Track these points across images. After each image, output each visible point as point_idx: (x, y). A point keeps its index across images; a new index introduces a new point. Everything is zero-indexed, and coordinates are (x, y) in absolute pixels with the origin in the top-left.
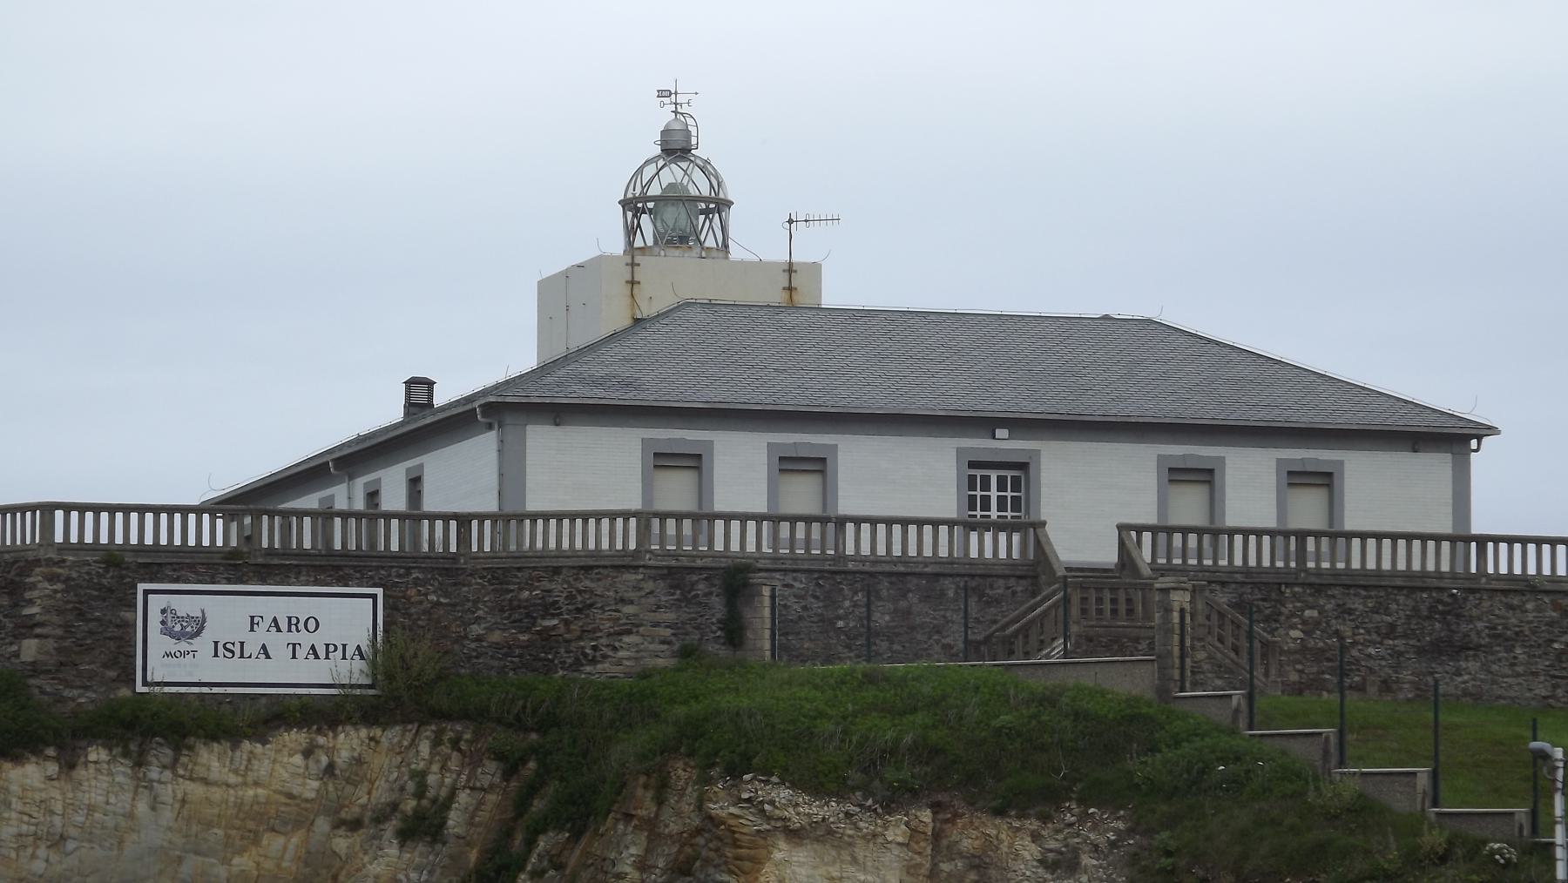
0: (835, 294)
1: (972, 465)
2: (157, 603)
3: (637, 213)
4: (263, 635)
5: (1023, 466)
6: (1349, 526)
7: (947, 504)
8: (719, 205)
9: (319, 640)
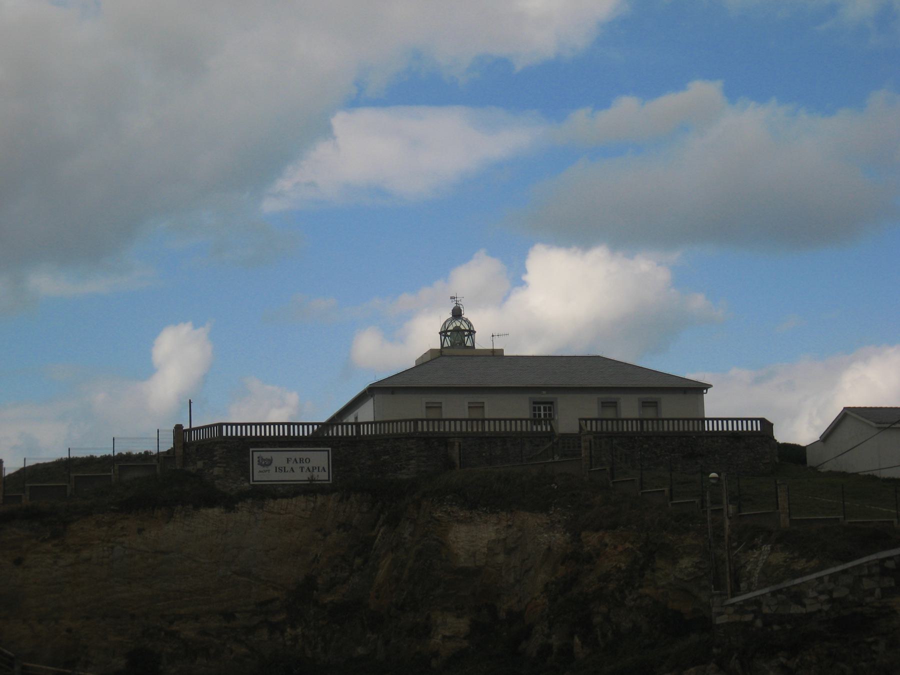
0: (505, 354)
1: (534, 403)
2: (257, 455)
3: (446, 336)
4: (291, 464)
5: (552, 403)
6: (663, 416)
7: (527, 413)
8: (471, 332)
9: (310, 465)
